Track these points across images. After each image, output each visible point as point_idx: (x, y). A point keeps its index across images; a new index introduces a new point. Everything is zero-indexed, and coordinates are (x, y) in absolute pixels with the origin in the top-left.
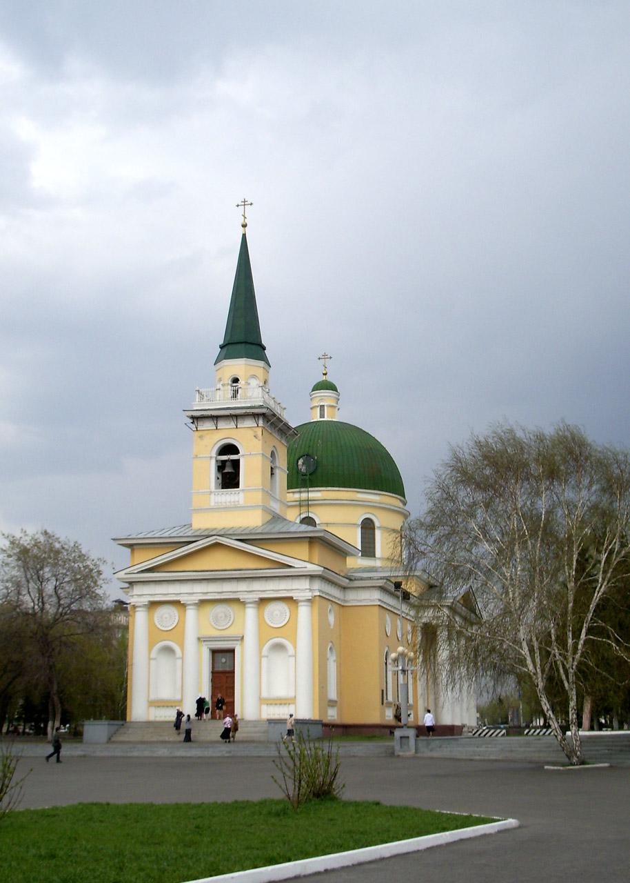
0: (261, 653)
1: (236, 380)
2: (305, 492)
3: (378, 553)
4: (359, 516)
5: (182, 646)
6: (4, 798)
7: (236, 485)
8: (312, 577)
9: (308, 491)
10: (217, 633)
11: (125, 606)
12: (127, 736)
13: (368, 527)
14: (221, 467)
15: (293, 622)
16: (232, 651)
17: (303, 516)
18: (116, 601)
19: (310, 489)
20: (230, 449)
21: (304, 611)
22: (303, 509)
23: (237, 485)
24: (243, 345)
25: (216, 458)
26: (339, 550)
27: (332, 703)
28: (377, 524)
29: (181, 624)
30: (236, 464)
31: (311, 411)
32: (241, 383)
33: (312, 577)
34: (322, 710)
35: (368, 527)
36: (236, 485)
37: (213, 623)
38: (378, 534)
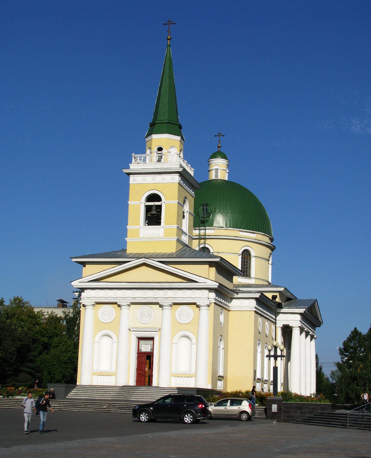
0: (172, 341)
1: (160, 149)
2: (203, 229)
3: (253, 274)
4: (240, 247)
5: (118, 335)
6: (364, 398)
7: (158, 222)
8: (210, 290)
9: (205, 229)
10: (143, 326)
11: (65, 304)
12: (72, 394)
13: (246, 255)
14: (148, 209)
15: (196, 322)
16: (152, 339)
17: (202, 246)
18: (59, 301)
19: (207, 228)
20: (154, 197)
21: (204, 311)
22: (202, 241)
23: (149, 224)
24: (166, 124)
25: (145, 203)
26: (95, 255)
27: (221, 378)
28: (253, 253)
29: (118, 320)
30: (159, 208)
31: (208, 172)
32: (164, 151)
33: (210, 290)
34: (214, 383)
35: (246, 255)
36: (158, 222)
37: (139, 319)
38: (253, 260)
